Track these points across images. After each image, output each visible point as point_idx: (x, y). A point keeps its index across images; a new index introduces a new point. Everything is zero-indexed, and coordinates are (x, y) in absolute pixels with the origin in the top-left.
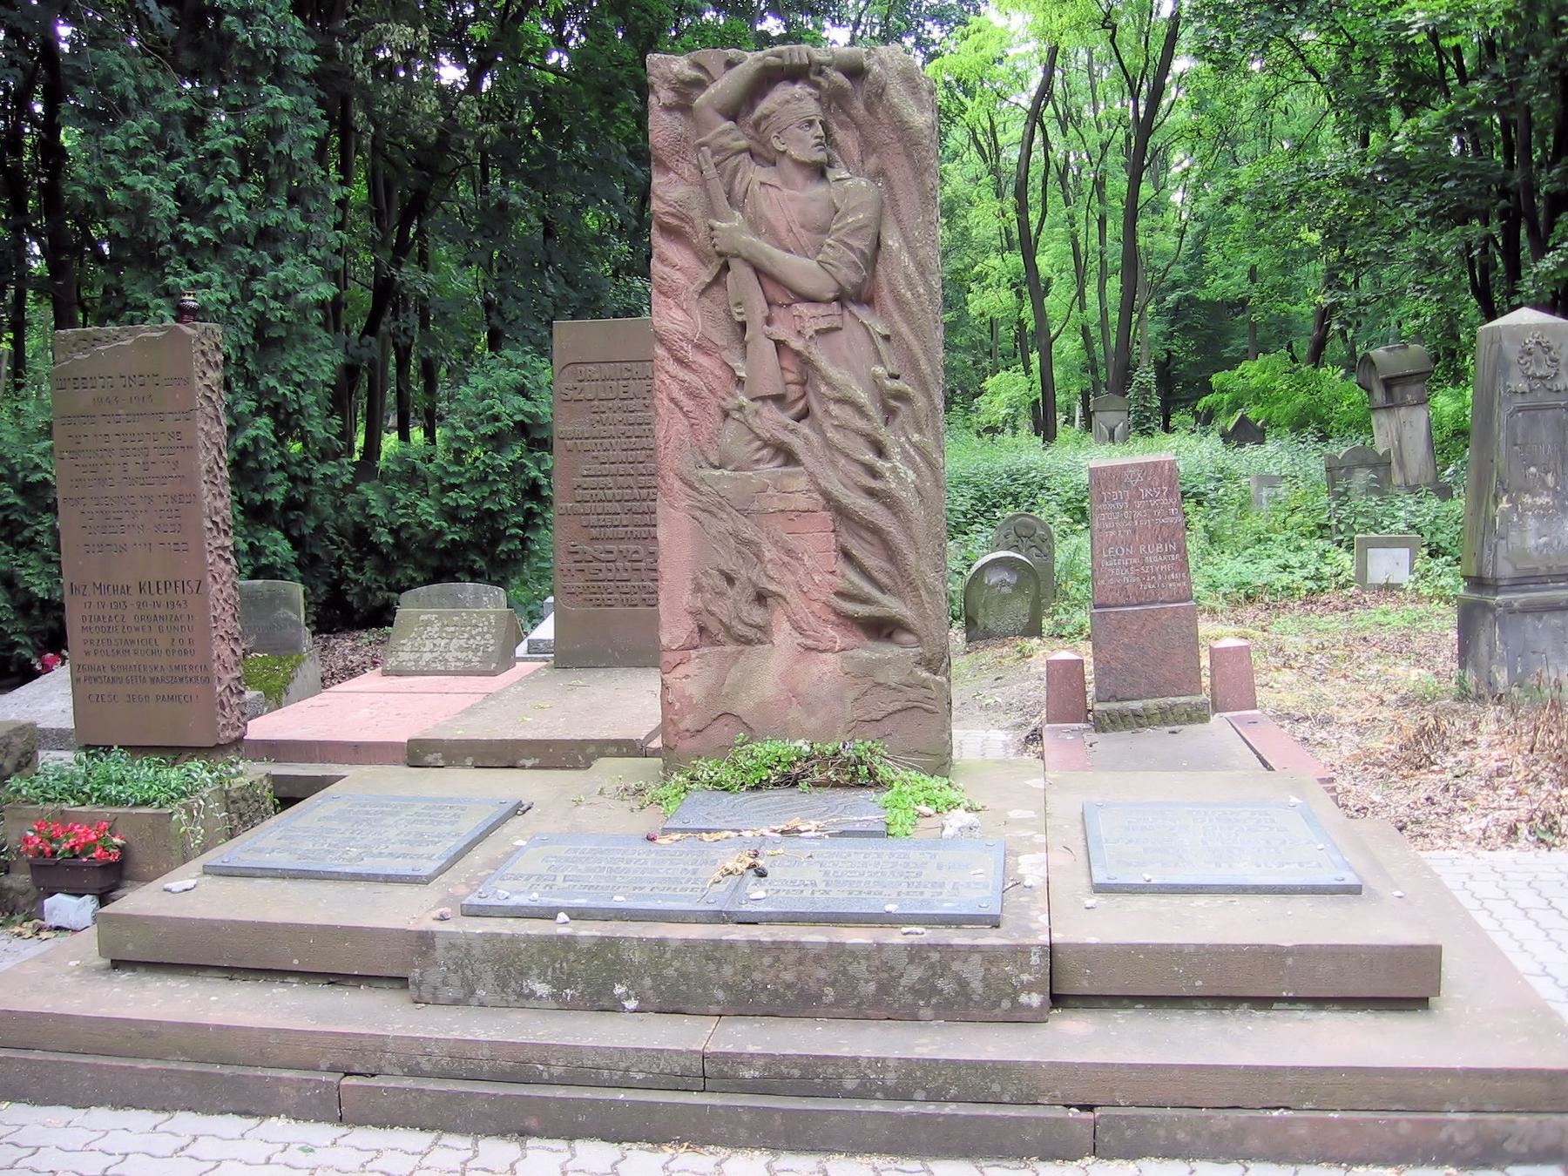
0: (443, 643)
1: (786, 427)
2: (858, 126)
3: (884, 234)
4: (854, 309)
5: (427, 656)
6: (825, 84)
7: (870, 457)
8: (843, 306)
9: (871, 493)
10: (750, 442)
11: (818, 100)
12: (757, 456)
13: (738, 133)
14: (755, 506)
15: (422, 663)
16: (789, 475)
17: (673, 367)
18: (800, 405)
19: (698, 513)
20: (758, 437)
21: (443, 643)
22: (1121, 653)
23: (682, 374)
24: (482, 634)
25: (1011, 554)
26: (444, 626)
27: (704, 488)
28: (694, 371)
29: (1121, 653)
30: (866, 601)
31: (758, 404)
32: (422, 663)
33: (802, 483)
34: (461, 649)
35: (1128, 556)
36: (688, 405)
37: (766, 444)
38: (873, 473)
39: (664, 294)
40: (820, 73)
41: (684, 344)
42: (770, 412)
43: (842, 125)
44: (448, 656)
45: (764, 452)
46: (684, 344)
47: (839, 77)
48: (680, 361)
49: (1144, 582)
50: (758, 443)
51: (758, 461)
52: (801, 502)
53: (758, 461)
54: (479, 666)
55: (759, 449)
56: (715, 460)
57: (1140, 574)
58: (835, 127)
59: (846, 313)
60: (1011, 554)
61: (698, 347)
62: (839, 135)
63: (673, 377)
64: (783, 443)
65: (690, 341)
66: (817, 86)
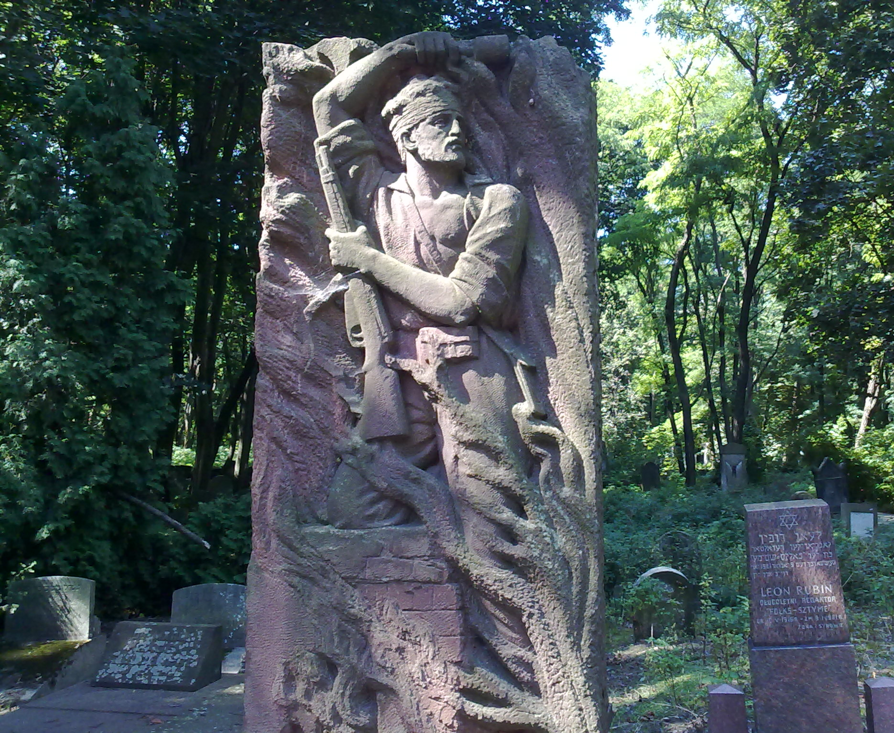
0: (151, 656)
1: (407, 475)
2: (504, 127)
3: (531, 248)
4: (494, 335)
5: (135, 669)
6: (464, 76)
7: (507, 515)
8: (480, 332)
9: (507, 561)
10: (362, 493)
11: (456, 94)
12: (371, 511)
13: (364, 132)
14: (368, 573)
15: (129, 676)
16: (409, 535)
17: (276, 400)
18: (428, 449)
19: (296, 580)
20: (373, 488)
21: (151, 656)
22: (781, 692)
23: (289, 409)
24: (188, 649)
25: (675, 571)
26: (155, 640)
27: (305, 549)
28: (303, 406)
29: (781, 692)
30: (503, 703)
31: (375, 447)
32: (129, 676)
33: (422, 547)
34: (167, 664)
35: (785, 596)
36: (292, 444)
37: (382, 496)
38: (510, 534)
39: (271, 314)
40: (459, 63)
41: (292, 374)
42: (390, 457)
43: (485, 126)
44: (153, 670)
45: (380, 506)
46: (292, 374)
47: (480, 67)
48: (287, 394)
49: (802, 622)
50: (373, 494)
51: (371, 518)
52: (423, 570)
53: (371, 518)
54: (179, 680)
55: (373, 502)
56: (325, 517)
57: (798, 615)
58: (477, 128)
59: (484, 340)
60: (675, 571)
61: (309, 378)
62: (481, 136)
63: (278, 413)
64: (402, 495)
65: (299, 370)
66: (455, 79)
